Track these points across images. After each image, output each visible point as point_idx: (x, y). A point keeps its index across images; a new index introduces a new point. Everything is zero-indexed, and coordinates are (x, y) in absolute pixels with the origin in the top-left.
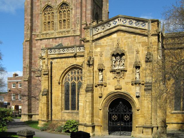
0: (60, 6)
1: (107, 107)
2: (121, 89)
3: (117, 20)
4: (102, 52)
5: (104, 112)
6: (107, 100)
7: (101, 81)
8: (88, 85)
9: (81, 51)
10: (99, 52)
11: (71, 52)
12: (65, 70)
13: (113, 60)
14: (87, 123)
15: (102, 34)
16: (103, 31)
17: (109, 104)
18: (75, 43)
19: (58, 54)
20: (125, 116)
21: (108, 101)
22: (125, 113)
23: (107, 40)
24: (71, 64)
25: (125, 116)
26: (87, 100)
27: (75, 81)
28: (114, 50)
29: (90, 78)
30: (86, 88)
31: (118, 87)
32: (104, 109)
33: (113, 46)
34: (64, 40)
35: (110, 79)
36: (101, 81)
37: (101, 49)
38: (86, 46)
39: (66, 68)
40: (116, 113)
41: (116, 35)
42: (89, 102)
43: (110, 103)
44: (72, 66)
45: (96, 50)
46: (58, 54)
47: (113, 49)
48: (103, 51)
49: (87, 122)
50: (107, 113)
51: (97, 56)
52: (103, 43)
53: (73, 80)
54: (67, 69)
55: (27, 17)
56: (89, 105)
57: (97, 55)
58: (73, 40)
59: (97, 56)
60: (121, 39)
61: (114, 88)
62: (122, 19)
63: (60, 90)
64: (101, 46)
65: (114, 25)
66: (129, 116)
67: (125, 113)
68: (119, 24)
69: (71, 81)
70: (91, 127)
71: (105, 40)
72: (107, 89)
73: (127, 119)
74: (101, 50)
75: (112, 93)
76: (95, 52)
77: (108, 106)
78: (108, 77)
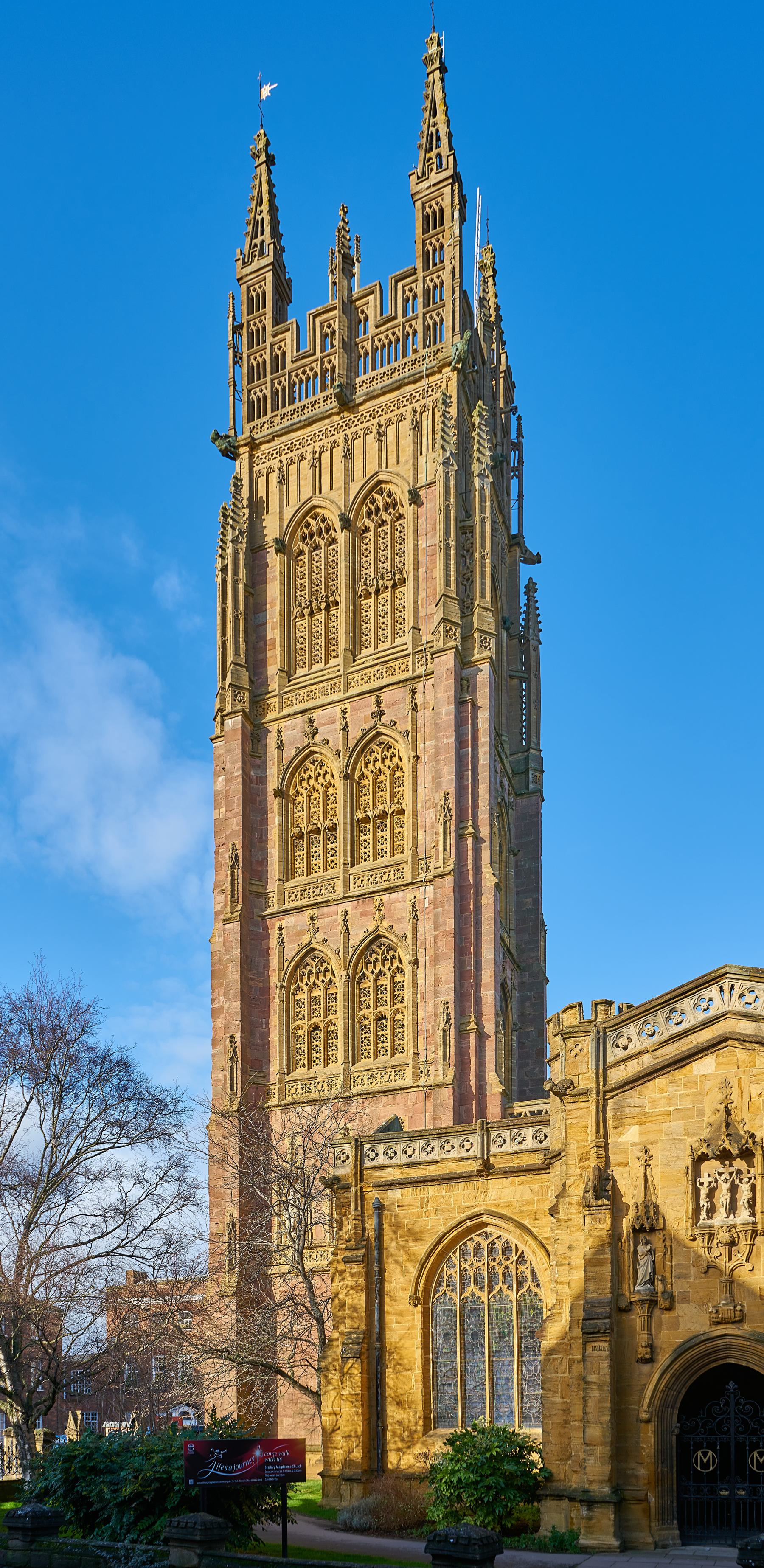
0: (362, 953)
1: (673, 1407)
2: (741, 1321)
3: (713, 992)
4: (649, 1147)
5: (660, 1435)
6: (672, 1376)
7: (646, 1283)
8: (592, 1306)
9: (507, 1148)
10: (633, 1145)
11: (464, 1154)
12: (438, 1243)
13: (702, 1184)
14: (595, 1487)
15: (647, 1061)
16: (648, 1043)
17: (681, 1396)
18: (435, 1119)
19: (408, 1165)
20: (700, 1453)
21: (677, 1378)
22: (754, 1439)
23: (671, 1089)
24: (462, 1209)
25: (700, 1453)
26: (593, 1378)
27: (478, 1293)
28: (705, 1134)
29: (597, 1269)
30: (584, 1319)
31: (727, 1310)
32: (661, 1419)
33: (701, 1114)
34: (381, 1105)
35: (686, 1276)
36: (646, 1283)
37: (642, 1133)
38: (574, 1121)
39: (442, 1229)
40: (712, 1438)
41: (714, 1065)
42: (600, 1386)
43: (684, 1391)
44: (471, 1218)
45: (623, 1139)
46: (408, 1165)
47: (702, 1129)
48: (653, 1143)
49: (591, 1482)
50: (674, 1437)
51: (627, 1165)
52: (654, 1102)
53: (472, 1288)
54: (445, 1234)
55: (227, 1005)
56: (599, 1401)
57: (624, 1161)
58: (420, 1105)
59: (627, 1165)
60: (736, 1080)
61: (706, 1319)
62: (737, 984)
63: (418, 1332)
64: (643, 1119)
65: (701, 1016)
66: (715, 1451)
67: (754, 1439)
68: (726, 1008)
69: (463, 1289)
70: (611, 1508)
71: (661, 1090)
72: (674, 1325)
73: (705, 1466)
74: (645, 1138)
75: (698, 1340)
76: (617, 1144)
77: (678, 1405)
78: (679, 1265)
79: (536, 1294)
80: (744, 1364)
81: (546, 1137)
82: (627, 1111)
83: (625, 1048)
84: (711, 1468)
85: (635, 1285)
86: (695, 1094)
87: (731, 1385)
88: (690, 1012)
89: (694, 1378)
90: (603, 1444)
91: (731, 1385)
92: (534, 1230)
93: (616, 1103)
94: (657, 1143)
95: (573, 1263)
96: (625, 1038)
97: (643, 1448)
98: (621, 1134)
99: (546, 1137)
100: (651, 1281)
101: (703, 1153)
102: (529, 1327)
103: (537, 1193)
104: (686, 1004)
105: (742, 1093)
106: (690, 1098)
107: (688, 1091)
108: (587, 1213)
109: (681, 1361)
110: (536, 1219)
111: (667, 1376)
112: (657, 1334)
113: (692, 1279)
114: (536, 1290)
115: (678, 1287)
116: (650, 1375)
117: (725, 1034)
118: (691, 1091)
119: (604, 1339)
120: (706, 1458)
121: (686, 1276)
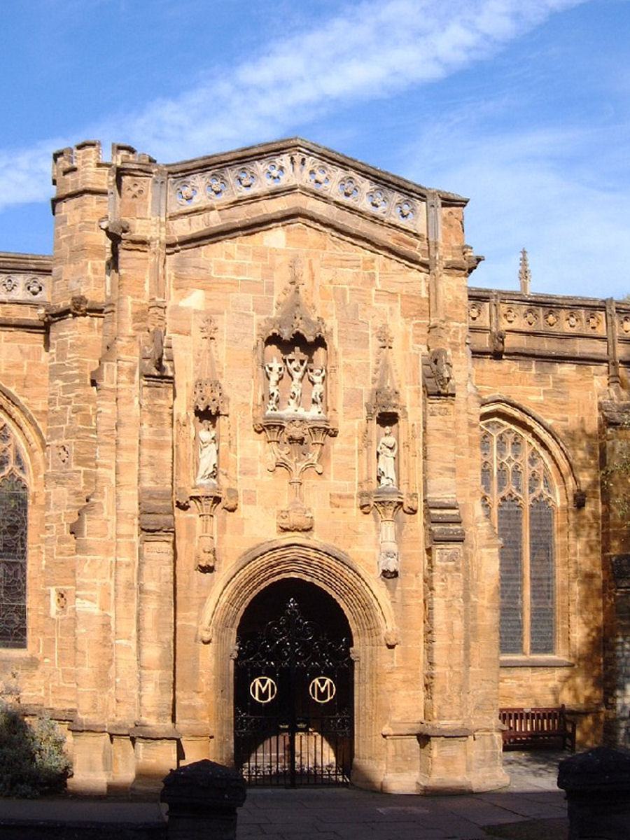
10: (196, 312)
20: (316, 681)
31: (295, 519)
33: (270, 290)
50: (232, 662)
52: (221, 268)
60: (307, 260)
64: (207, 285)
71: (229, 256)
72: (239, 529)
79: (20, 480)
80: (308, 579)
81: (40, 289)
82: (191, 271)
83: (189, 199)
84: (329, 699)
85: (195, 478)
86: (264, 267)
87: (292, 603)
88: (262, 177)
89: (255, 592)
90: (161, 667)
91: (292, 603)
92: (22, 400)
93: (178, 260)
94: (222, 313)
95: (122, 442)
96: (325, 176)
97: (202, 674)
98: (183, 297)
99: (40, 289)
100: (214, 475)
101: (274, 334)
102: (10, 521)
103: (27, 355)
104: (260, 167)
105: (313, 276)
106: (260, 271)
107: (257, 263)
108: (146, 383)
109: (247, 570)
110: (25, 386)
111: (231, 587)
112: (219, 538)
113: (259, 477)
114: (20, 474)
115: (242, 484)
116: (210, 586)
117: (296, 208)
118: (260, 263)
119: (167, 539)
120: (263, 687)
121: (253, 473)
